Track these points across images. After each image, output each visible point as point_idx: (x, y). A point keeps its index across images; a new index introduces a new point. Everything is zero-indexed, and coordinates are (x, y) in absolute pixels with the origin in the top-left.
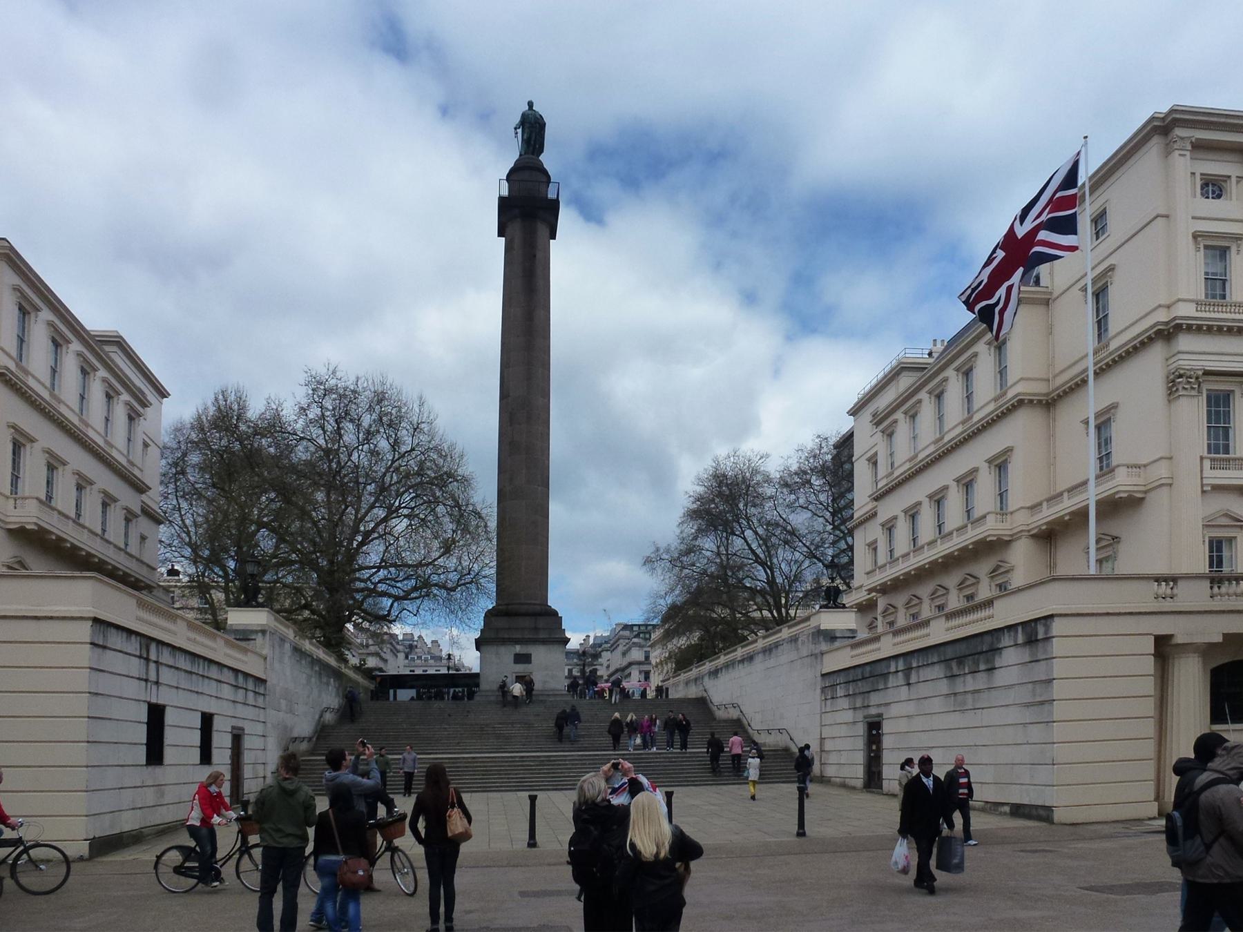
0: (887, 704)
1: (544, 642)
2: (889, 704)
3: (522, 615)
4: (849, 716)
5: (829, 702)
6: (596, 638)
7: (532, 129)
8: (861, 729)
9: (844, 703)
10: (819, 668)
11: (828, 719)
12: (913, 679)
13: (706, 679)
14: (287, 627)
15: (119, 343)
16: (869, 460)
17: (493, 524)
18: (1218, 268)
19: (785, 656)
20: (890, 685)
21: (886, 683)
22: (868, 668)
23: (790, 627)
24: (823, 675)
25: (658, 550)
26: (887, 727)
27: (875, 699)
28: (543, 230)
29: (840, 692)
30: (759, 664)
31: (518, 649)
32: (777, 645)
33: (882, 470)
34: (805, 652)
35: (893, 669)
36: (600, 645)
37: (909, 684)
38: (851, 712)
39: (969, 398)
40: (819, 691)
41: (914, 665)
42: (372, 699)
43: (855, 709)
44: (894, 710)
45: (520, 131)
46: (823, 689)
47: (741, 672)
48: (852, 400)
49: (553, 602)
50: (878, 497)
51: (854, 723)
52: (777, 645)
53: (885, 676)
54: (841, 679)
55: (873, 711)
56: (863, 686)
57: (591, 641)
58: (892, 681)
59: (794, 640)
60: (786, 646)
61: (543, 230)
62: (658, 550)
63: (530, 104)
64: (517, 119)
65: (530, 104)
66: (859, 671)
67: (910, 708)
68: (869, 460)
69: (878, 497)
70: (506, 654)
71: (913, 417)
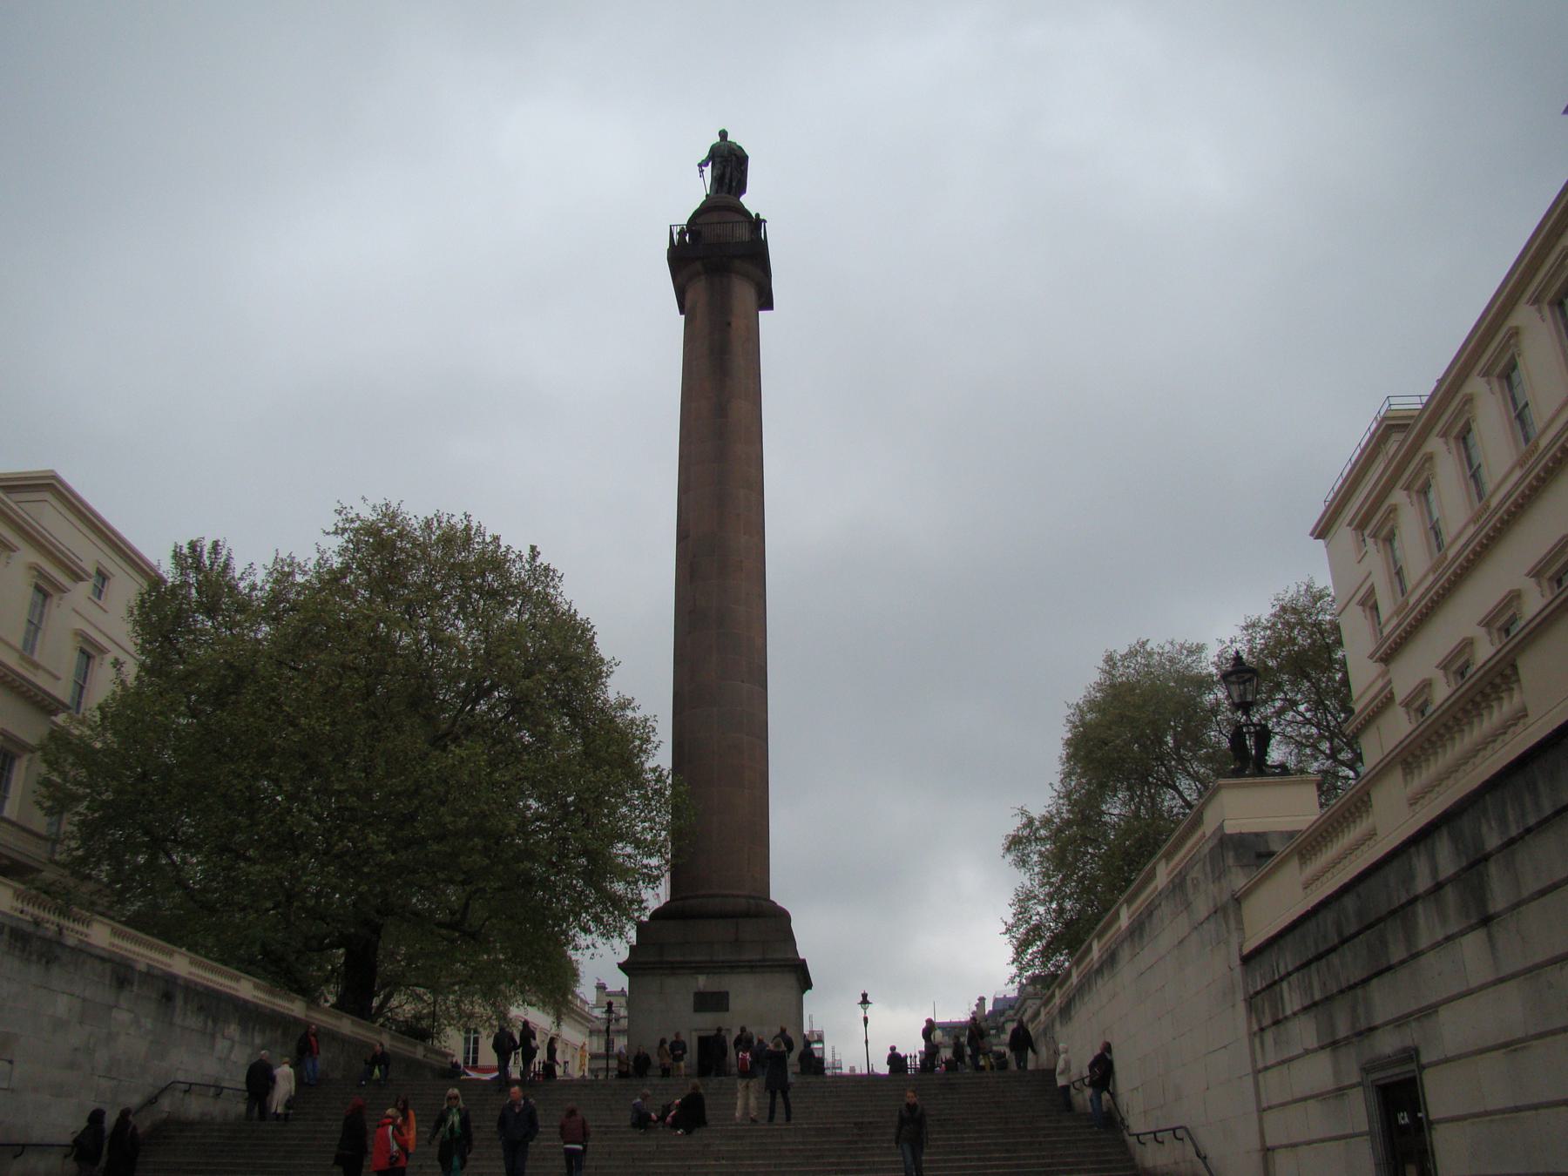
0: (1430, 1011)
1: (752, 967)
2: (1430, 1011)
3: (727, 926)
4: (1318, 1072)
5: (1269, 1036)
6: (996, 1001)
7: (728, 165)
8: (1359, 1112)
9: (1304, 1033)
10: (1234, 940)
11: (1276, 1087)
12: (1499, 899)
13: (1057, 1026)
14: (171, 954)
15: (49, 486)
16: (1362, 603)
17: (661, 757)
18: (698, 266)
19: (1169, 930)
20: (1423, 942)
21: (1410, 934)
22: (1349, 902)
23: (1168, 856)
24: (1247, 960)
25: (1031, 821)
26: (1442, 1095)
27: (1385, 1001)
28: (743, 292)
29: (1292, 1000)
30: (1126, 970)
31: (702, 982)
32: (1150, 911)
33: (1386, 609)
34: (1202, 907)
35: (1423, 883)
36: (1002, 1013)
37: (1486, 921)
38: (1324, 1059)
39: (1520, 417)
40: (1241, 1008)
41: (1493, 841)
42: (634, 1125)
43: (1334, 1045)
44: (1454, 1029)
45: (708, 170)
46: (1251, 1001)
47: (1103, 988)
48: (1315, 512)
49: (780, 892)
50: (1388, 655)
51: (1340, 1092)
52: (1150, 911)
53: (1403, 912)
54: (1286, 960)
55: (1387, 1044)
56: (1349, 965)
57: (989, 1007)
58: (1428, 928)
59: (1178, 885)
60: (1165, 909)
61: (743, 292)
62: (1031, 821)
63: (723, 134)
64: (704, 154)
65: (723, 134)
66: (1329, 917)
67: (1506, 1012)
68: (1362, 603)
69: (1388, 655)
70: (680, 992)
71: (1424, 491)
